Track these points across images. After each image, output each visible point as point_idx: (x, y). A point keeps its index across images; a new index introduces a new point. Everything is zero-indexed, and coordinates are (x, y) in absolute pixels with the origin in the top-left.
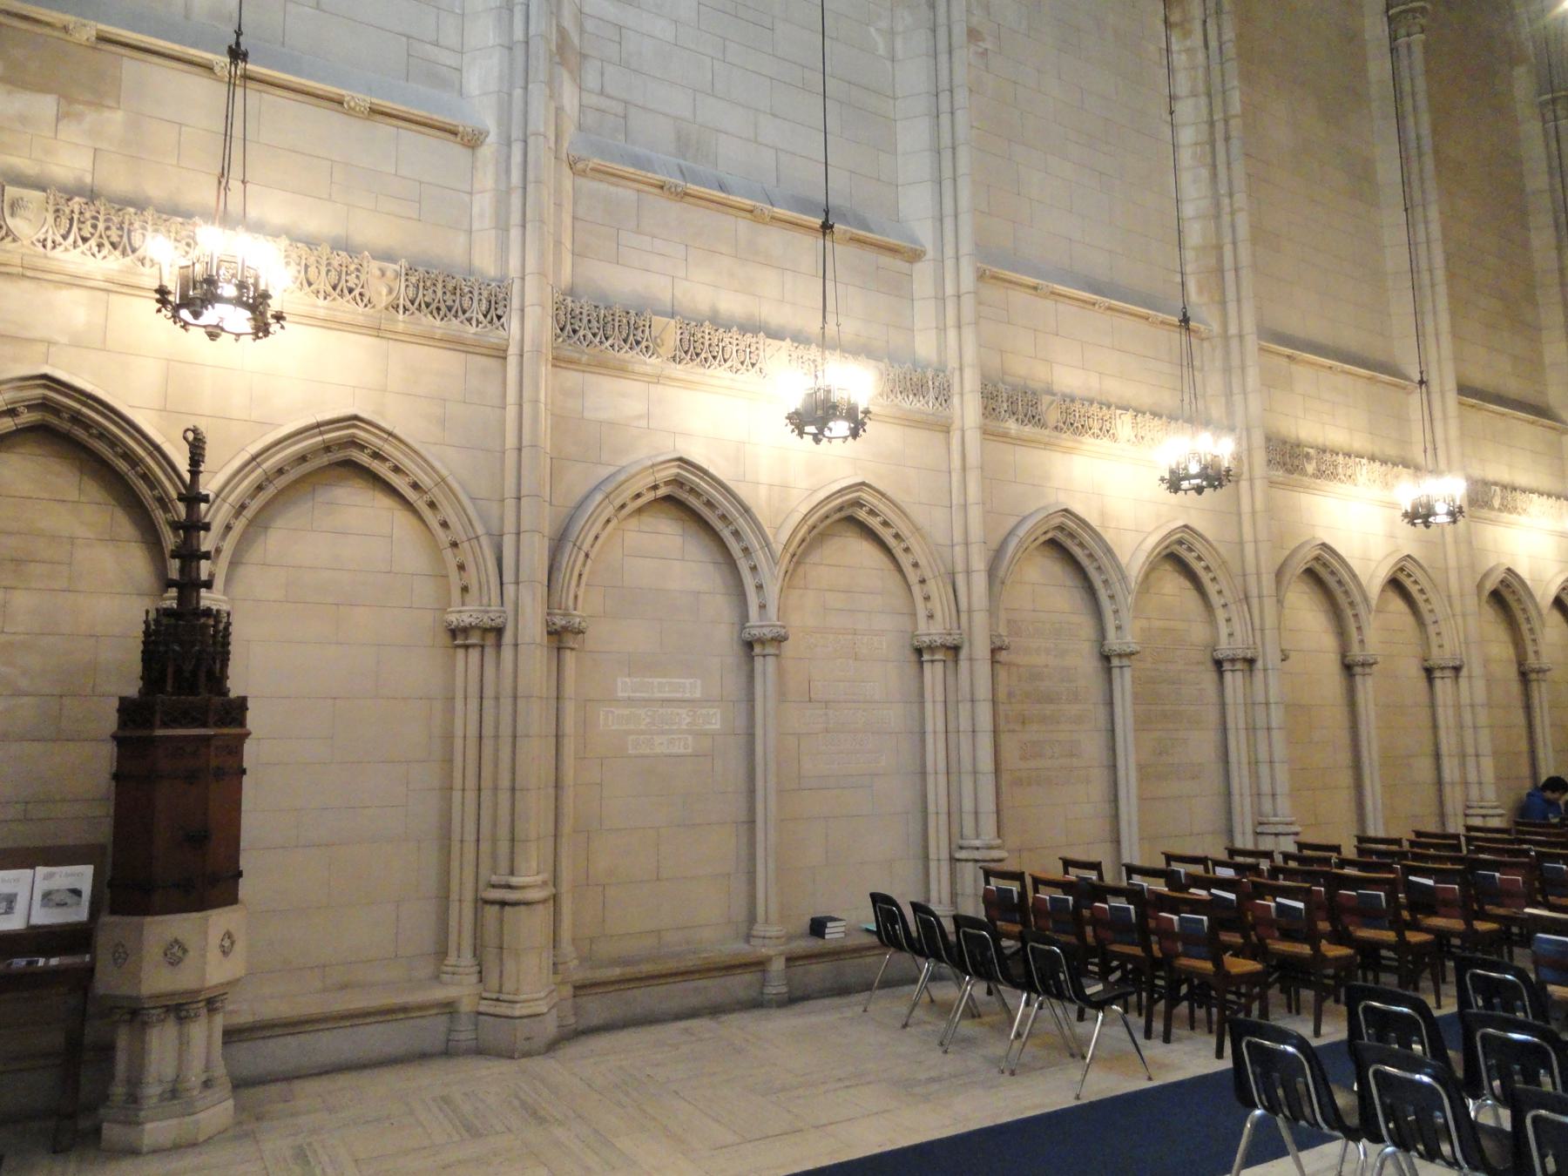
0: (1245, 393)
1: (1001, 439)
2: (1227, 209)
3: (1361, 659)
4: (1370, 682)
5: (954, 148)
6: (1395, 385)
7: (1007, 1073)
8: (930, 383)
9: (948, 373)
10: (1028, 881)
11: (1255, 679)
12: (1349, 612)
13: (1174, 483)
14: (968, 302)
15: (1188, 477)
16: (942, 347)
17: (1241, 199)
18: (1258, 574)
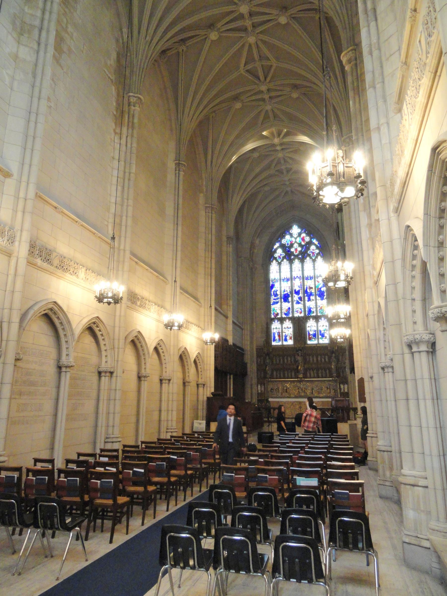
0: (123, 271)
1: (33, 266)
2: (125, 204)
3: (144, 374)
4: (146, 382)
5: (34, 138)
6: (163, 281)
7: (16, 575)
8: (6, 233)
9: (15, 230)
10: (24, 471)
11: (112, 379)
12: (143, 357)
13: (100, 299)
14: (30, 204)
15: (107, 297)
16: (14, 218)
17: (131, 202)
18: (119, 340)
